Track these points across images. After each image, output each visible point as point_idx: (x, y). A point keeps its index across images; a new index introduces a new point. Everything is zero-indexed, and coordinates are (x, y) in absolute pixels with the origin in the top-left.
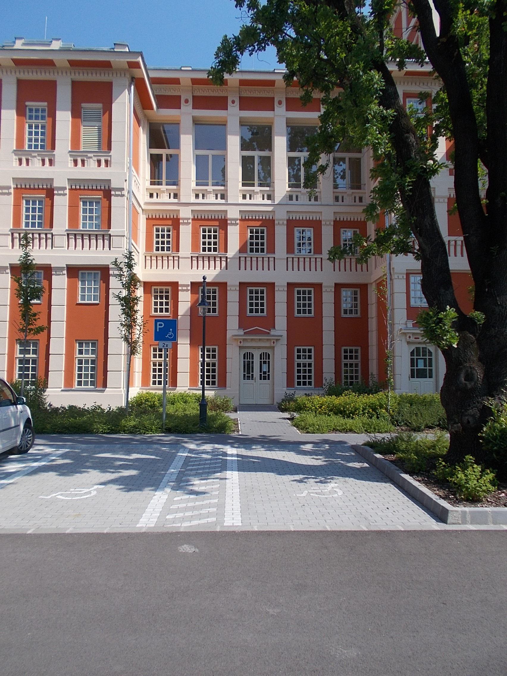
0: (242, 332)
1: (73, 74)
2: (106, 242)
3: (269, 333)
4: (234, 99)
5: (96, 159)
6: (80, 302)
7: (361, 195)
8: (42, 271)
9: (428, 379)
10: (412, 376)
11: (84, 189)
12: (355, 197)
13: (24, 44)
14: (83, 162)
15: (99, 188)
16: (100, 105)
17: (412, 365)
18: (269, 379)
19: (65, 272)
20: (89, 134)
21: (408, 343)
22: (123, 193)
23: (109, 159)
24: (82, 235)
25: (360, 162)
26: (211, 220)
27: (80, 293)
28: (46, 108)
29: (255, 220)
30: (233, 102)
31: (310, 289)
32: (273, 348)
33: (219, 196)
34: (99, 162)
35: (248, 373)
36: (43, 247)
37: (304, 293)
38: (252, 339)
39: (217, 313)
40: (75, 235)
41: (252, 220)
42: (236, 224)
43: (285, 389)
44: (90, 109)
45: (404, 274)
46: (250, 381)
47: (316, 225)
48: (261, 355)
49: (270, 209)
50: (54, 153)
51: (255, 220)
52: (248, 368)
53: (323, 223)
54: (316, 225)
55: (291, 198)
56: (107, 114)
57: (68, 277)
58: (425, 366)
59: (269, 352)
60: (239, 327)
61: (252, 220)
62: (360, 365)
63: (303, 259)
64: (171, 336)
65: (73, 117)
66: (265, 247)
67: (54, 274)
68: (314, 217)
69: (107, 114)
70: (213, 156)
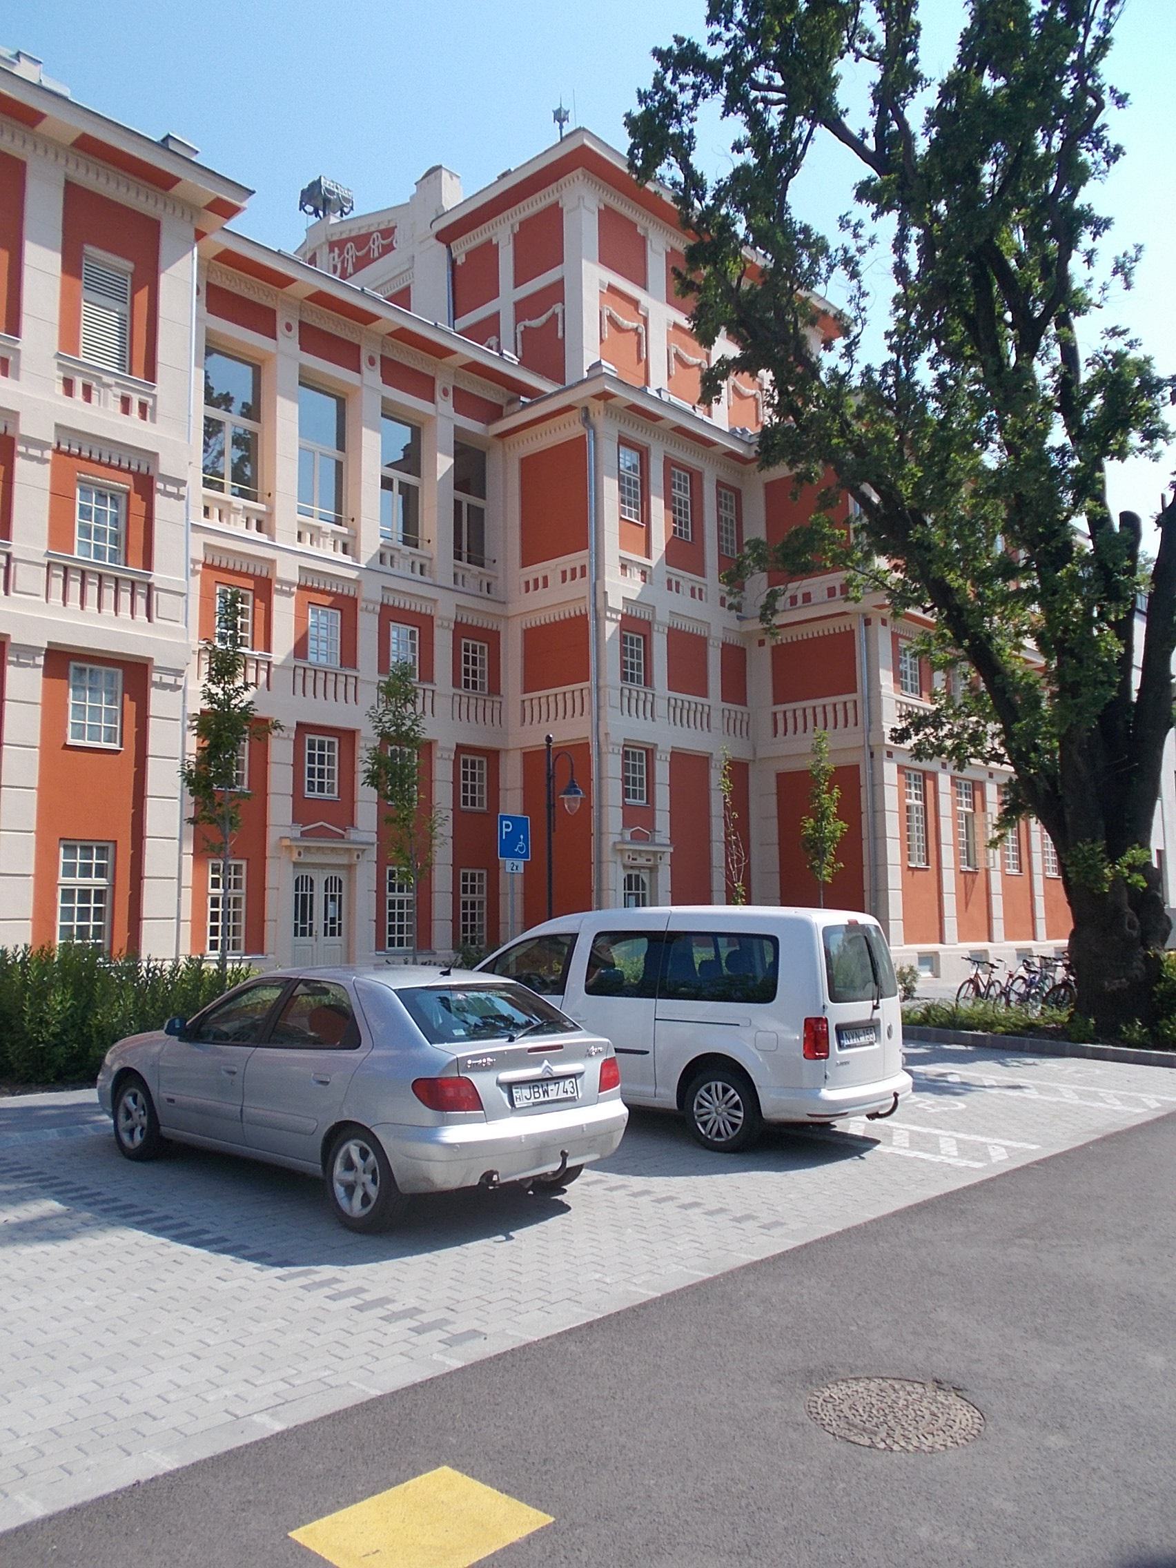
1: (72, 166)
2: (141, 602)
3: (343, 837)
5: (119, 391)
6: (71, 741)
8: (120, 671)
11: (89, 460)
14: (87, 390)
15: (125, 465)
16: (128, 266)
18: (311, 935)
19: (40, 660)
20: (101, 324)
22: (183, 491)
23: (150, 401)
24: (83, 573)
26: (239, 574)
27: (70, 720)
28: (129, 278)
29: (323, 592)
30: (289, 327)
31: (332, 739)
32: (350, 868)
33: (254, 522)
34: (126, 402)
35: (304, 921)
36: (91, 606)
38: (319, 848)
39: (336, 795)
40: (66, 569)
41: (317, 591)
42: (290, 594)
43: (373, 954)
44: (104, 264)
46: (307, 939)
48: (297, 881)
49: (353, 574)
50: (18, 346)
51: (323, 592)
52: (303, 907)
56: (143, 296)
57: (46, 675)
59: (342, 875)
60: (294, 822)
61: (317, 591)
62: (244, 901)
64: (521, 849)
67: (12, 663)
68: (425, 608)
69: (143, 296)
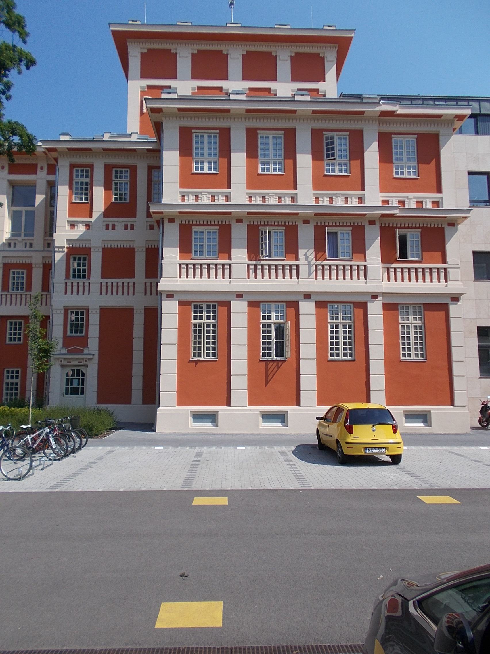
0: (64, 351)
4: (42, 165)
7: (31, 242)
9: (80, 395)
10: (67, 393)
12: (26, 244)
13: (110, 137)
17: (67, 384)
21: (62, 366)
25: (406, 237)
37: (16, 324)
39: (84, 334)
45: (97, 309)
47: (29, 267)
53: (33, 266)
54: (29, 267)
55: (10, 245)
58: (79, 385)
63: (20, 296)
65: (105, 189)
66: (24, 286)
68: (26, 261)
70: (26, 211)
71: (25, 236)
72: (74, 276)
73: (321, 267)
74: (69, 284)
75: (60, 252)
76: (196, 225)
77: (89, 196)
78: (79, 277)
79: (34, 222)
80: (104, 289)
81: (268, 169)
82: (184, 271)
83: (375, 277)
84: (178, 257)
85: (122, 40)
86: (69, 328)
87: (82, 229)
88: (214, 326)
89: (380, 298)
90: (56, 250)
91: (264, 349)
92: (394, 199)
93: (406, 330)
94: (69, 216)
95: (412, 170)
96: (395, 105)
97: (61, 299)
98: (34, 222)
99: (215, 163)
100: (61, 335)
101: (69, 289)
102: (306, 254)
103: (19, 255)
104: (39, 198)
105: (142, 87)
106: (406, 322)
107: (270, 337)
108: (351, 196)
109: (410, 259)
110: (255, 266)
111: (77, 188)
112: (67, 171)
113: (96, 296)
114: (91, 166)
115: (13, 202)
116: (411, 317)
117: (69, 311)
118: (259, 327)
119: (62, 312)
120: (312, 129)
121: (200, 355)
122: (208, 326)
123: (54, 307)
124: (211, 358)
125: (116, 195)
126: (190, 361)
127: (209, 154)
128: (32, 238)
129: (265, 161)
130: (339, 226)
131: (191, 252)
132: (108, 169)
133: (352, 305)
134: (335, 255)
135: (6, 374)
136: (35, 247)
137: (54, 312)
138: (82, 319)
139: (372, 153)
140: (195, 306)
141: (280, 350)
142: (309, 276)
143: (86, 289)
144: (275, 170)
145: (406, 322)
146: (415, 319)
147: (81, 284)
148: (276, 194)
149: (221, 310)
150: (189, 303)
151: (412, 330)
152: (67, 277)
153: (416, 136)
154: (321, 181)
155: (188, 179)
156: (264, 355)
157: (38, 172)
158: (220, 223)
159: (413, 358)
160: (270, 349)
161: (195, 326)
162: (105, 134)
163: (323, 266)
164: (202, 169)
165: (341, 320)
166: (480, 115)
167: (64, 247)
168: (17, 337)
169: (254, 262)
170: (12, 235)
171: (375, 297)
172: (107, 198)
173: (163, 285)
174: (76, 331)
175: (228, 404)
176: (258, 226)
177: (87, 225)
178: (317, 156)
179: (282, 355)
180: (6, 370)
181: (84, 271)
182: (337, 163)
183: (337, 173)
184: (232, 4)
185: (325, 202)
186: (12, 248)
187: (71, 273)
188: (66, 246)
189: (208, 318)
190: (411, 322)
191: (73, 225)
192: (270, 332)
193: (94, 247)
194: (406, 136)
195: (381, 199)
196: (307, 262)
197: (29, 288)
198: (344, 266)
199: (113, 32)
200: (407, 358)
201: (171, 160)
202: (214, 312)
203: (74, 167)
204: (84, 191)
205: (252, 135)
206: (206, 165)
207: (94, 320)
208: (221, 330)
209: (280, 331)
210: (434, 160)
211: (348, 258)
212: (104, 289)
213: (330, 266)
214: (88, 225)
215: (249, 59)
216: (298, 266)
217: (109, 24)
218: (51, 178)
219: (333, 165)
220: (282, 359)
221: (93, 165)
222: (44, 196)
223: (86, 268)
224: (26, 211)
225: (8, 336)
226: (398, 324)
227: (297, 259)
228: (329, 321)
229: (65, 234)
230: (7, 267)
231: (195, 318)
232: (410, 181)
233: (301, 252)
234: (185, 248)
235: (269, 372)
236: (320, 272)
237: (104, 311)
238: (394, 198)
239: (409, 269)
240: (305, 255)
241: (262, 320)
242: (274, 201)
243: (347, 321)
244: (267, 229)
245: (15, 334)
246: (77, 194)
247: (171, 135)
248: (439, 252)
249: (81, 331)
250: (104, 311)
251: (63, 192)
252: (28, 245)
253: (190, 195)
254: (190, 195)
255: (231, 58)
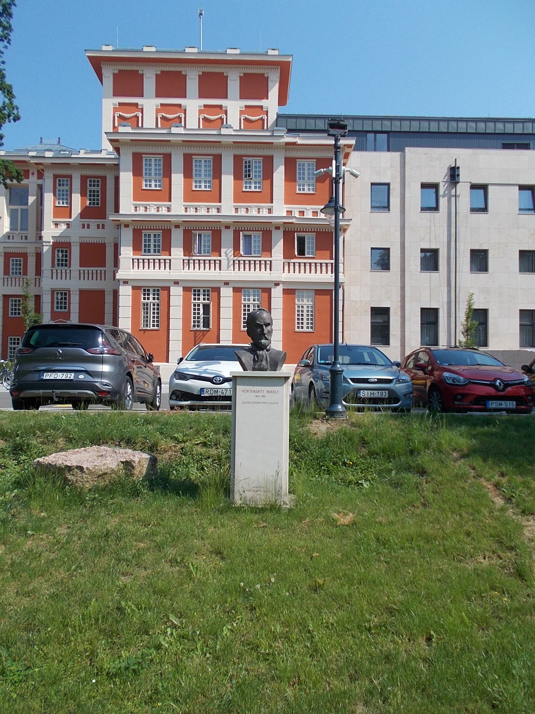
12: (22, 237)
13: (85, 153)
47: (25, 256)
53: (28, 255)
54: (25, 256)
71: (21, 229)
72: (58, 265)
73: (237, 262)
74: (54, 271)
75: (47, 246)
76: (145, 229)
77: (69, 201)
78: (62, 265)
79: (27, 220)
80: (82, 275)
81: (200, 186)
82: (136, 264)
83: (277, 269)
84: (132, 254)
85: (97, 64)
86: (55, 305)
87: (64, 227)
88: (158, 305)
89: (281, 285)
90: (44, 244)
91: (194, 322)
92: (296, 210)
93: (300, 309)
94: (54, 217)
95: (311, 187)
96: (295, 137)
97: (49, 283)
98: (27, 220)
99: (160, 181)
100: (49, 310)
101: (55, 275)
102: (227, 252)
103: (16, 246)
104: (32, 199)
105: (114, 104)
106: (301, 303)
107: (199, 314)
108: (263, 207)
109: (307, 256)
110: (189, 260)
111: (59, 195)
112: (52, 180)
113: (76, 280)
114: (70, 177)
115: (11, 202)
116: (305, 300)
117: (55, 292)
118: (191, 306)
119: (50, 292)
120: (234, 155)
121: (147, 326)
122: (154, 305)
123: (43, 289)
124: (156, 328)
125: (90, 200)
126: (140, 330)
127: (156, 174)
128: (27, 232)
129: (198, 180)
130: (253, 230)
131: (141, 250)
132: (84, 179)
133: (260, 290)
134: (248, 252)
135: (9, 341)
136: (28, 240)
137: (44, 292)
138: (65, 299)
139: (279, 174)
140: (144, 290)
141: (206, 323)
142: (228, 268)
143: (68, 275)
144: (205, 187)
145: (301, 303)
146: (308, 301)
147: (64, 271)
148: (205, 206)
149: (163, 293)
150: (141, 288)
151: (305, 309)
152: (53, 265)
153: (315, 160)
154: (240, 196)
155: (140, 194)
156: (194, 326)
157: (30, 176)
158: (163, 228)
159: (305, 329)
160: (199, 322)
161: (144, 304)
162: (81, 151)
163: (239, 261)
164: (150, 186)
165: (252, 301)
166: (391, 131)
167: (50, 242)
168: (17, 311)
169: (187, 258)
170: (11, 229)
171: (277, 284)
172: (83, 202)
173: (120, 275)
174: (61, 308)
175: (168, 361)
176: (191, 230)
177: (67, 224)
178: (238, 176)
179: (208, 327)
180: (9, 337)
181: (66, 261)
182: (253, 182)
183: (253, 189)
184: (201, 14)
185: (242, 212)
186: (11, 240)
187: (56, 262)
188: (52, 241)
189: (154, 299)
190: (305, 303)
191: (56, 224)
192: (199, 309)
193: (74, 243)
194: (307, 160)
195: (285, 210)
196: (226, 258)
197: (25, 273)
198: (255, 261)
199: (89, 57)
200: (300, 330)
201: (127, 179)
202: (158, 295)
203: (57, 177)
204: (65, 197)
205: (188, 159)
206: (153, 183)
207: (75, 299)
208: (163, 308)
209: (206, 307)
210: (328, 179)
211: (259, 255)
212: (82, 275)
213: (244, 261)
214: (68, 225)
215: (204, 79)
216: (220, 261)
217: (85, 50)
218: (40, 182)
219: (250, 183)
220: (207, 329)
221: (72, 176)
222: (35, 197)
223: (68, 258)
224: (22, 210)
225: (10, 311)
226: (191, 303)
227: (220, 256)
228: (243, 302)
229: (51, 232)
230: (7, 256)
231: (195, 299)
232: (309, 196)
233: (223, 251)
234: (137, 248)
235: (197, 339)
236: (237, 266)
237: (83, 293)
238: (296, 209)
239: (305, 263)
240: (226, 253)
241: (193, 301)
242: (203, 212)
243: (256, 302)
244: (198, 232)
245: (15, 310)
246: (59, 199)
247: (127, 161)
248: (328, 250)
249: (65, 308)
250: (83, 293)
251: (49, 198)
252: (24, 238)
253: (141, 207)
254: (141, 207)
255: (189, 79)
